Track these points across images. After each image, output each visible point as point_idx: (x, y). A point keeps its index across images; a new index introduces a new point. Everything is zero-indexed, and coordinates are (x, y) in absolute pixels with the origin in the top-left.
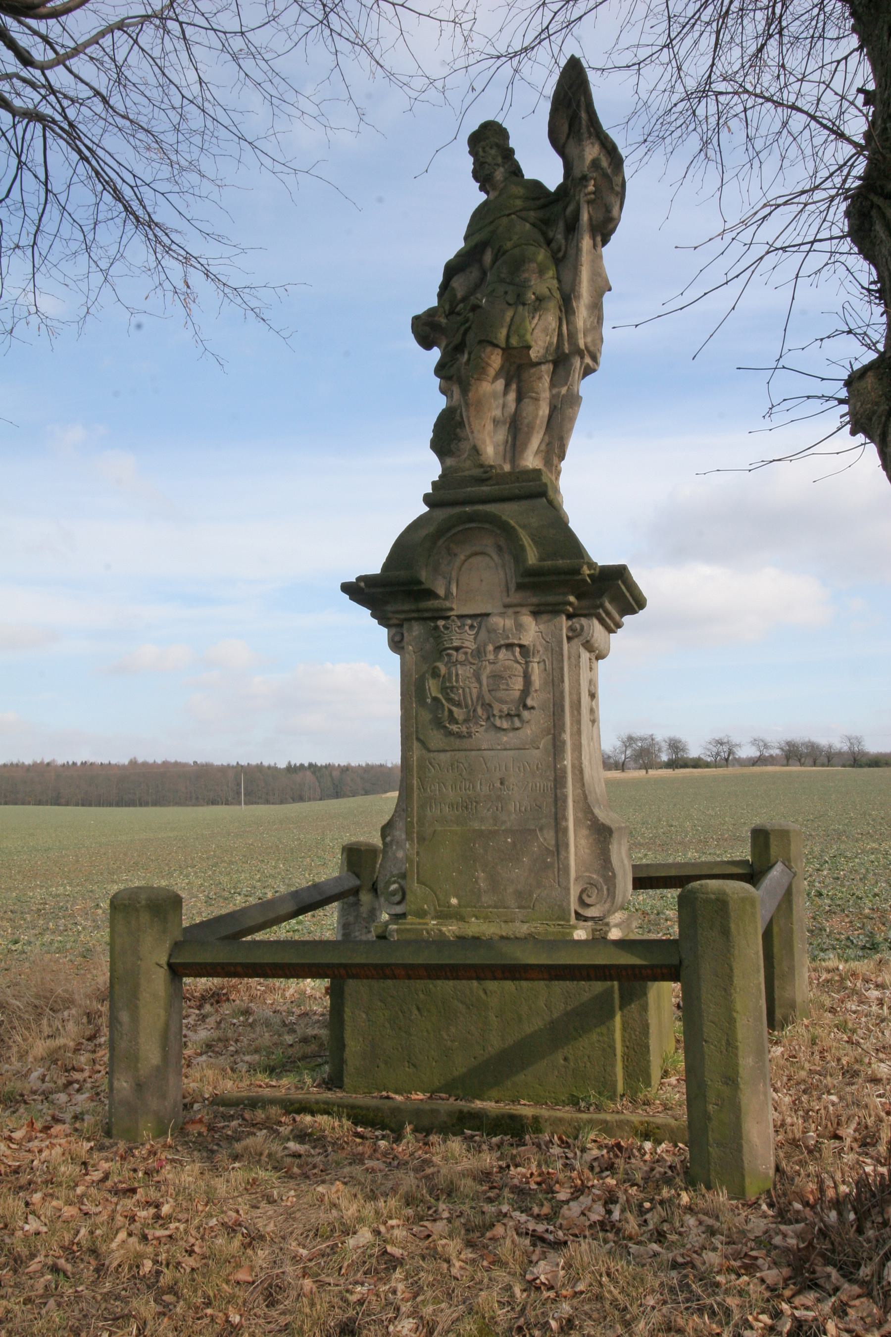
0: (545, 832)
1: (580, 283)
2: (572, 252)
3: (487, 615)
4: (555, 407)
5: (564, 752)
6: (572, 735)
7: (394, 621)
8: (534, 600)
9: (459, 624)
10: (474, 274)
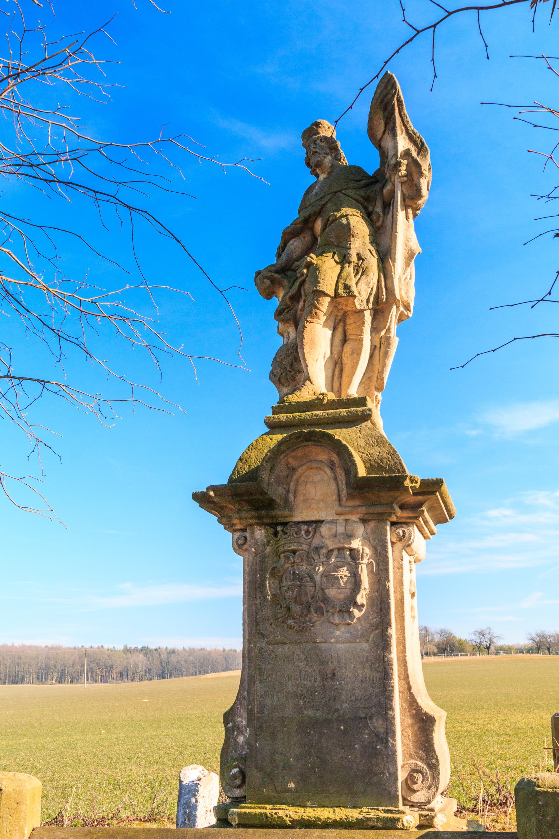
0: (374, 720)
1: (395, 247)
2: (389, 222)
4: (375, 346)
5: (391, 645)
6: (397, 630)
7: (239, 527)
8: (363, 510)
10: (306, 238)
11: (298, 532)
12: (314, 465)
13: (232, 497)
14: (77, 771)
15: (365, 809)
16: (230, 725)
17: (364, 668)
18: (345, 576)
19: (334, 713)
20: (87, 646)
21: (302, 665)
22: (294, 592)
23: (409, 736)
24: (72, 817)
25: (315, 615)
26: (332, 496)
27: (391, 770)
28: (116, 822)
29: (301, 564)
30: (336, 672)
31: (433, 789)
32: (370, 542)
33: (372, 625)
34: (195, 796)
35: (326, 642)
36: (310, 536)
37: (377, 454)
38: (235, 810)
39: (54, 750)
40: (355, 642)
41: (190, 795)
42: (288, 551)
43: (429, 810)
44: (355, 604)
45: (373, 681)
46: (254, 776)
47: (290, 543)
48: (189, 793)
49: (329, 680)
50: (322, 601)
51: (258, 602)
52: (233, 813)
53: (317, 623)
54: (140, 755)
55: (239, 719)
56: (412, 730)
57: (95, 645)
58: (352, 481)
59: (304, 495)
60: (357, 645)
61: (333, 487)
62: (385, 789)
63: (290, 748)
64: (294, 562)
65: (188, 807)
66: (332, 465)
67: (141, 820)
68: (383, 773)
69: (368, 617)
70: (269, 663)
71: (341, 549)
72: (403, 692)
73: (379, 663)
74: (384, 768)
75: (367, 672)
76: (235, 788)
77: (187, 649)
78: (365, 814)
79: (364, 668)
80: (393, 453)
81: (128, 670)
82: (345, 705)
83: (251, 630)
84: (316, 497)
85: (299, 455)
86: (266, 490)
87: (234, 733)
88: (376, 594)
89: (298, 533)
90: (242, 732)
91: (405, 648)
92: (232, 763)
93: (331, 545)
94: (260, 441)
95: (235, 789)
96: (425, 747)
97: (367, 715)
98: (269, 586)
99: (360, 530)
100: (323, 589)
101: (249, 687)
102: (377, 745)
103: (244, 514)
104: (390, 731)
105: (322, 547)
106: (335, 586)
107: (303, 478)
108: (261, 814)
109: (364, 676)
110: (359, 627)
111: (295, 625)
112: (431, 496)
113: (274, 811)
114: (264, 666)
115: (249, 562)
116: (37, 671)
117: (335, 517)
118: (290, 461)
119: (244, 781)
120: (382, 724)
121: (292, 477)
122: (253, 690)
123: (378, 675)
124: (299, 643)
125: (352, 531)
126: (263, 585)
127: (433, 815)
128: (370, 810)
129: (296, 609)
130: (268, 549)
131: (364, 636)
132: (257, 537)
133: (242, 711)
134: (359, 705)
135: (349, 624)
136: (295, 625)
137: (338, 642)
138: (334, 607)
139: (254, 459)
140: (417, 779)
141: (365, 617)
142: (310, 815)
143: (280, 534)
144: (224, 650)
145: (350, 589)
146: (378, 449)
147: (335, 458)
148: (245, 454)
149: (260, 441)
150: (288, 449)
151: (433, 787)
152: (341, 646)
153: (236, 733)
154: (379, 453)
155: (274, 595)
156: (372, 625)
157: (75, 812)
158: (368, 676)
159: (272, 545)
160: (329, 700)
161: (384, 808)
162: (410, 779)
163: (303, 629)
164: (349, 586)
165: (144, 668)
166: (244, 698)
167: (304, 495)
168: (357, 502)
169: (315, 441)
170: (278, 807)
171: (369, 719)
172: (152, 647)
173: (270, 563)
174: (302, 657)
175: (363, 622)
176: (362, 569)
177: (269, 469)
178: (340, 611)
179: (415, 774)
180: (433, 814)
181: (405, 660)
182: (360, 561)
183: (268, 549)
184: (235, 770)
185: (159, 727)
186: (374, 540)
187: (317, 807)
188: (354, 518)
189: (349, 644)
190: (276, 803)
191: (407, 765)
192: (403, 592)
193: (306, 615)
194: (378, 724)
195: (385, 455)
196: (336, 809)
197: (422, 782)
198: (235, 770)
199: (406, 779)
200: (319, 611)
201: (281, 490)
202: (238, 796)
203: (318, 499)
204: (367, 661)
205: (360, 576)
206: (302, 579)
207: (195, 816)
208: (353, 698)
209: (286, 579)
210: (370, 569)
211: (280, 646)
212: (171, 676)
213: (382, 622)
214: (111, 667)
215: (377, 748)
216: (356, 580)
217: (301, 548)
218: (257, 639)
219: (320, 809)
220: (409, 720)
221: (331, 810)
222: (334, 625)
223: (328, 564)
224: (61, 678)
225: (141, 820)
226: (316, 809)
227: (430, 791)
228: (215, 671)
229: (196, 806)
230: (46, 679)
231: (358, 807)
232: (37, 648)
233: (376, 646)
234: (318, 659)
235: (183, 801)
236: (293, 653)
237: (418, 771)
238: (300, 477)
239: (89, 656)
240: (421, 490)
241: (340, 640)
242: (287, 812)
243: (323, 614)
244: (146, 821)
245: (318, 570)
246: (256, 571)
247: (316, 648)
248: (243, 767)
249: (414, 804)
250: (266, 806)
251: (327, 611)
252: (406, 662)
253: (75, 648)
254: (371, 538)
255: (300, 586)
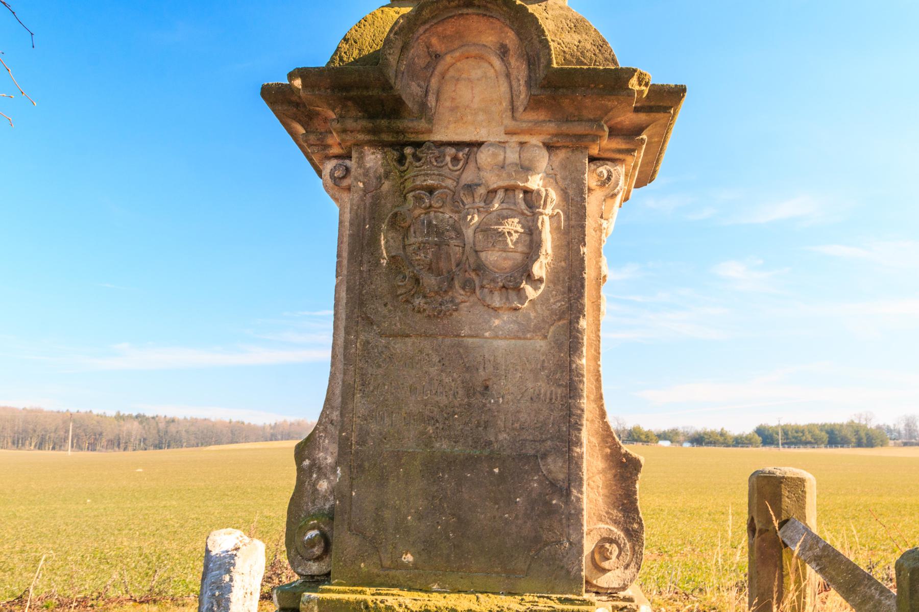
0: (550, 460)
3: (479, 144)
7: (336, 150)
8: (552, 127)
9: (437, 154)
11: (440, 158)
12: (473, 51)
13: (333, 90)
14: (55, 543)
15: (528, 597)
16: (307, 463)
17: (536, 379)
18: (516, 232)
19: (483, 448)
20: (73, 410)
21: (434, 371)
22: (427, 253)
23: (598, 487)
24: (43, 595)
25: (462, 292)
26: (501, 103)
27: (573, 537)
28: (103, 603)
29: (441, 210)
30: (489, 383)
31: (632, 569)
32: (557, 183)
33: (553, 313)
34: (229, 571)
35: (477, 336)
36: (459, 167)
37: (577, 43)
38: (313, 595)
39: (28, 519)
40: (525, 339)
41: (222, 571)
42: (422, 188)
43: (625, 599)
44: (529, 277)
45: (551, 399)
46: (347, 542)
47: (427, 175)
48: (219, 568)
49: (478, 395)
50: (474, 270)
51: (364, 268)
52: (310, 600)
53: (463, 305)
54: (132, 526)
55: (321, 454)
56: (603, 478)
57: (83, 410)
58: (541, 74)
59: (453, 99)
60: (528, 343)
61: (504, 88)
62: (562, 567)
63: (408, 501)
64: (431, 206)
65: (218, 588)
66: (503, 52)
67: (135, 601)
68: (559, 542)
69: (548, 300)
70: (380, 366)
71: (509, 190)
72: (592, 420)
73: (563, 372)
74: (561, 534)
75: (543, 387)
76: (310, 560)
77: (189, 418)
78: (528, 605)
79: (536, 379)
80: (602, 45)
81: (119, 439)
82: (503, 436)
83: (352, 312)
84: (475, 100)
85: (448, 33)
86: (392, 81)
87: (311, 476)
88: (563, 264)
89: (439, 160)
90: (325, 475)
91: (599, 353)
92: (309, 521)
93: (494, 181)
94: (379, 14)
95: (311, 563)
96: (623, 504)
97: (537, 452)
98: (386, 243)
99: (543, 160)
100: (476, 252)
101: (344, 403)
102: (552, 500)
103: (350, 124)
104: (574, 478)
105: (480, 185)
106: (498, 247)
107: (452, 73)
108: (358, 602)
109: (537, 391)
110: (532, 315)
111: (426, 306)
112: (661, 115)
113: (380, 598)
114: (370, 370)
115: (352, 205)
116: (12, 435)
117: (504, 138)
118: (434, 41)
119: (327, 550)
120: (562, 467)
121: (434, 69)
122: (350, 407)
123: (559, 391)
124: (430, 336)
125: (531, 161)
126: (374, 241)
127: (635, 608)
128: (536, 599)
129: (430, 281)
130: (386, 186)
131: (539, 329)
132: (368, 165)
133: (327, 441)
134: (525, 435)
135: (516, 309)
136: (426, 306)
137: (496, 337)
138: (494, 280)
139: (369, 39)
140: (611, 553)
141: (544, 299)
142: (439, 604)
143: (410, 159)
144: (230, 422)
145: (522, 253)
146: (577, 37)
147: (510, 38)
148: (354, 31)
149: (379, 14)
150: (433, 18)
151: (632, 564)
152: (502, 343)
153: (315, 476)
154: (579, 42)
155: (393, 257)
156: (553, 313)
157: (47, 590)
158: (542, 391)
159: (394, 179)
160: (477, 427)
161: (559, 596)
162: (600, 553)
163: (440, 314)
164: (520, 248)
165: (138, 437)
166: (332, 422)
167: (453, 99)
168: (542, 115)
169: (479, 7)
170: (384, 590)
171: (542, 459)
172: (149, 414)
173: (388, 206)
174: (435, 359)
175: (538, 307)
176: (543, 222)
177: (400, 46)
178: (504, 287)
179: (607, 545)
180: (633, 605)
181: (599, 371)
182: (541, 210)
183: (386, 186)
184: (313, 533)
185: (155, 498)
186: (564, 179)
187: (449, 593)
188: (535, 140)
189: (513, 341)
190: (381, 585)
191: (595, 532)
192: (600, 267)
193: (446, 292)
194: (555, 467)
195: (589, 46)
196: (480, 595)
197: (618, 557)
198: (313, 533)
199: (593, 552)
200: (468, 285)
201: (415, 88)
202: (316, 573)
203: (476, 106)
204: (543, 368)
205: (540, 232)
206: (443, 233)
207: (228, 600)
208: (517, 425)
209: (415, 233)
210: (555, 225)
211: (399, 339)
212: (169, 447)
213: (570, 308)
214: (101, 434)
215: (551, 504)
216: (531, 241)
217: (443, 184)
218: (360, 327)
219: (454, 596)
220: (599, 463)
221: (473, 597)
222: (491, 310)
223: (487, 211)
224: (41, 444)
225: (135, 601)
226: (447, 595)
227: (627, 572)
228: (218, 443)
229: (231, 586)
230: (23, 444)
231: (515, 594)
232: (13, 410)
233: (559, 345)
234: (461, 362)
235: (211, 578)
236: (421, 352)
237: (611, 541)
238: (448, 69)
239: (74, 421)
240: (646, 104)
241: (501, 334)
242: (401, 599)
243: (474, 292)
244: (141, 602)
245: (471, 220)
246: (364, 220)
247: (459, 345)
248: (326, 529)
249: (600, 591)
250: (364, 589)
251: (482, 287)
252: (600, 376)
253: (58, 412)
254: (558, 177)
255: (438, 245)
